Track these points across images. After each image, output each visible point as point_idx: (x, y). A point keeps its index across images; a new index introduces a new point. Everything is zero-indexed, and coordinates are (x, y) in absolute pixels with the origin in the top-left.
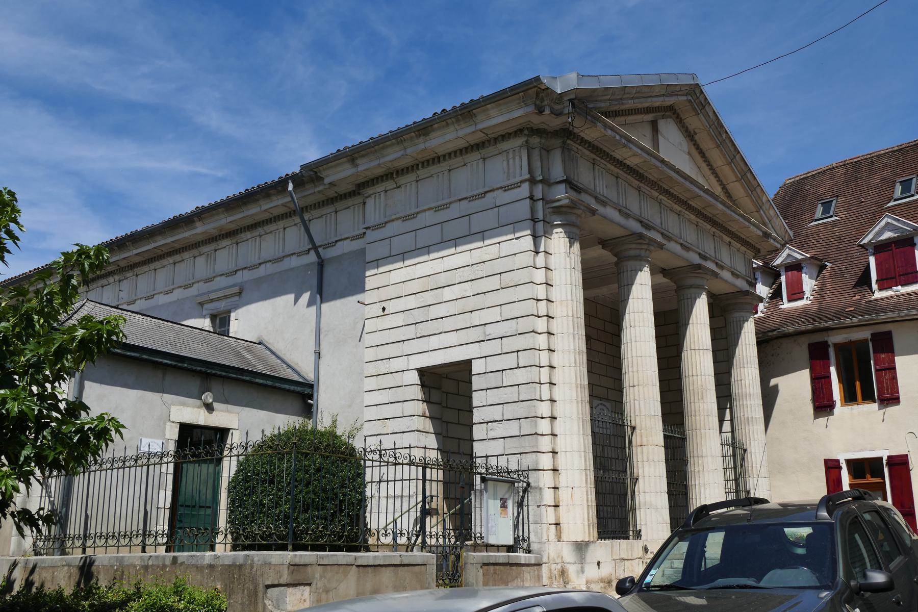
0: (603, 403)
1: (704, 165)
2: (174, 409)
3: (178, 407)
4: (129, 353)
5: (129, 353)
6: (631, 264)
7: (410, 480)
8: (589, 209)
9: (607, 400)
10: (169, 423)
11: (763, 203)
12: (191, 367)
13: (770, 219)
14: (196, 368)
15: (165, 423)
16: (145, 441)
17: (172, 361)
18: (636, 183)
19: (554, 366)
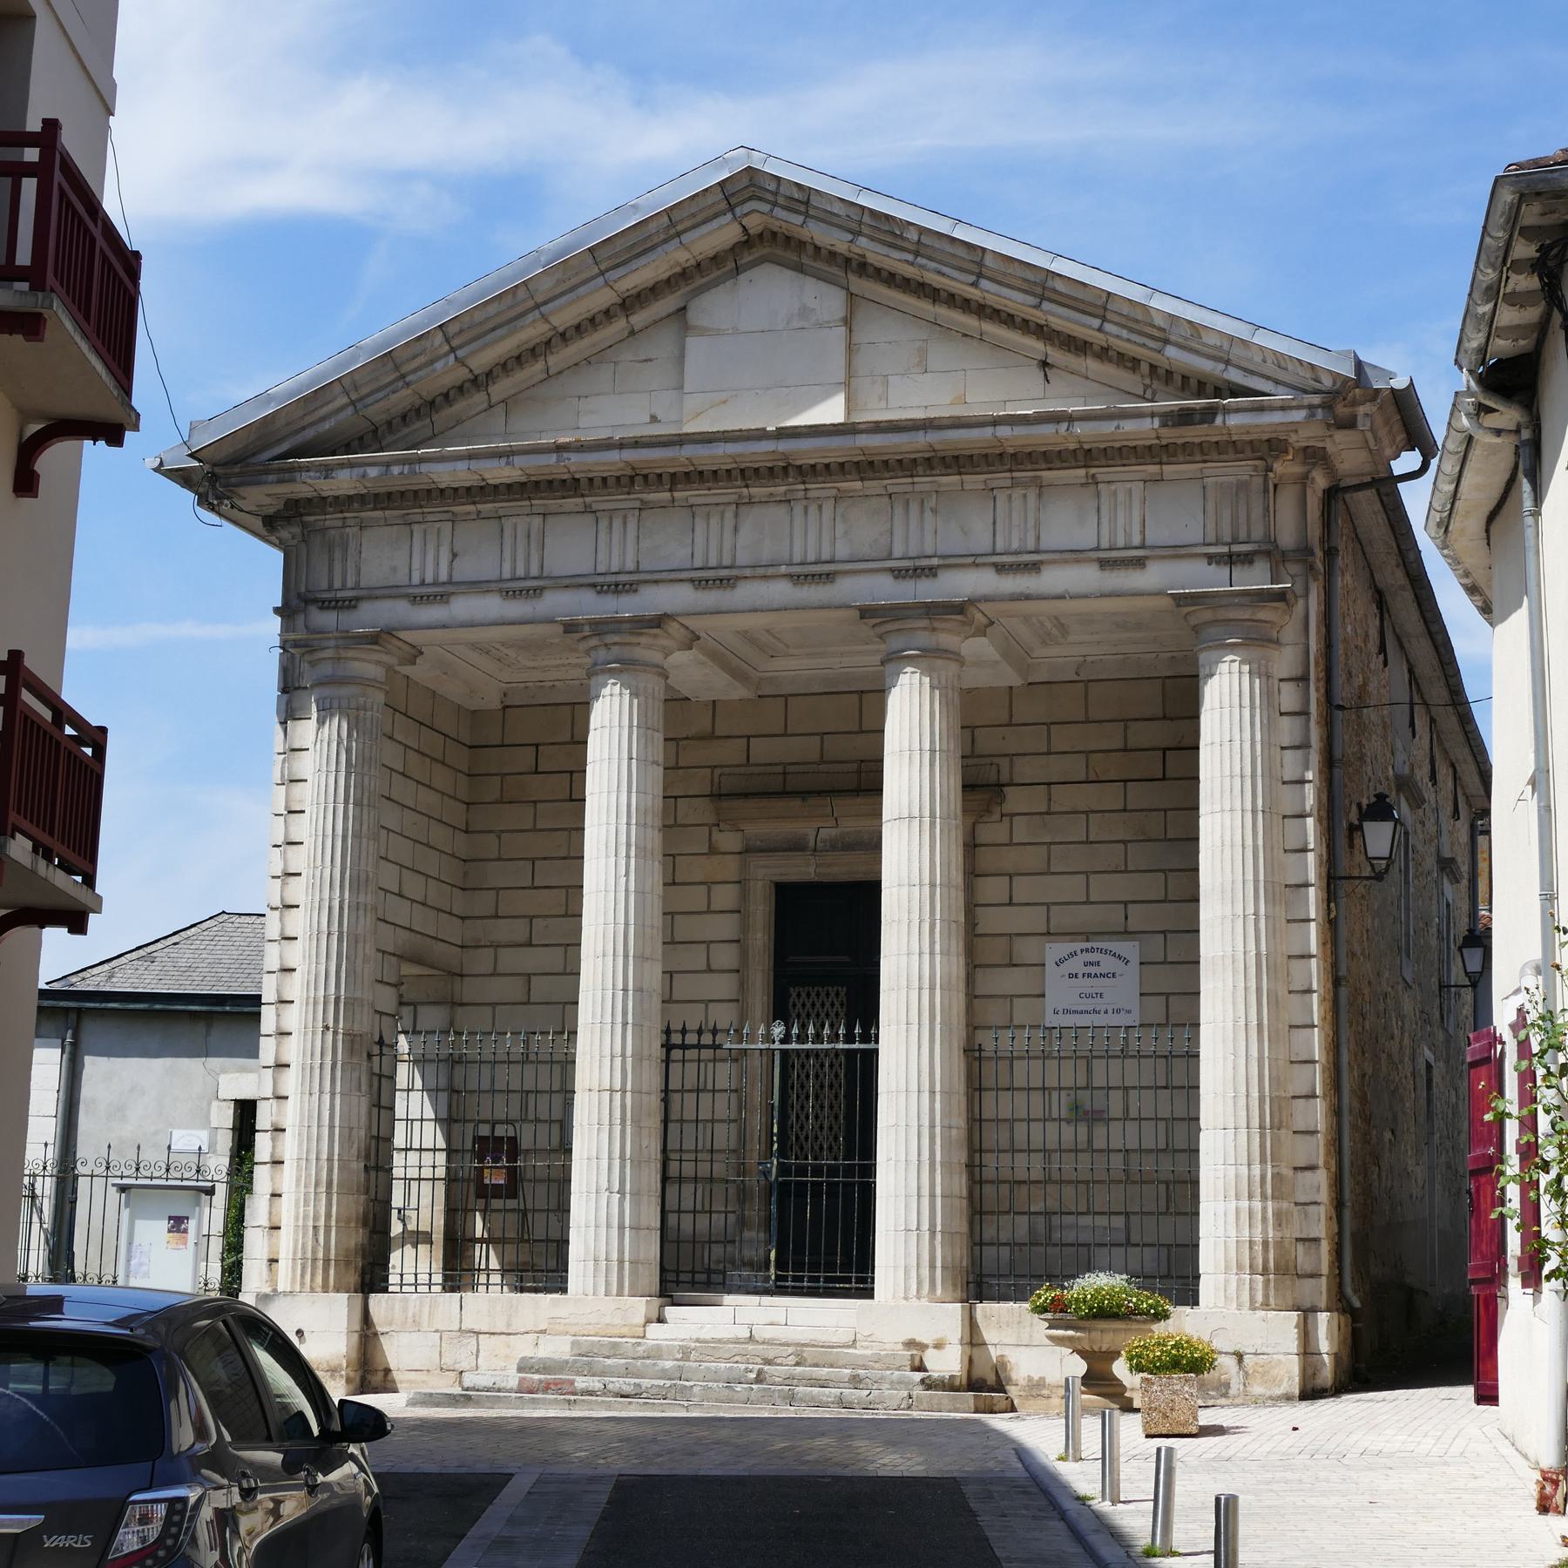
0: (1095, 945)
1: (943, 312)
2: (223, 1079)
3: (231, 1076)
4: (132, 1006)
5: (132, 1006)
6: (600, 678)
7: (1077, 1151)
8: (353, 637)
9: (1126, 933)
10: (215, 1103)
11: (1164, 330)
12: (236, 1009)
13: (1225, 356)
14: (246, 1010)
15: (209, 1104)
16: (177, 1134)
17: (202, 1005)
18: (573, 503)
19: (291, 965)
